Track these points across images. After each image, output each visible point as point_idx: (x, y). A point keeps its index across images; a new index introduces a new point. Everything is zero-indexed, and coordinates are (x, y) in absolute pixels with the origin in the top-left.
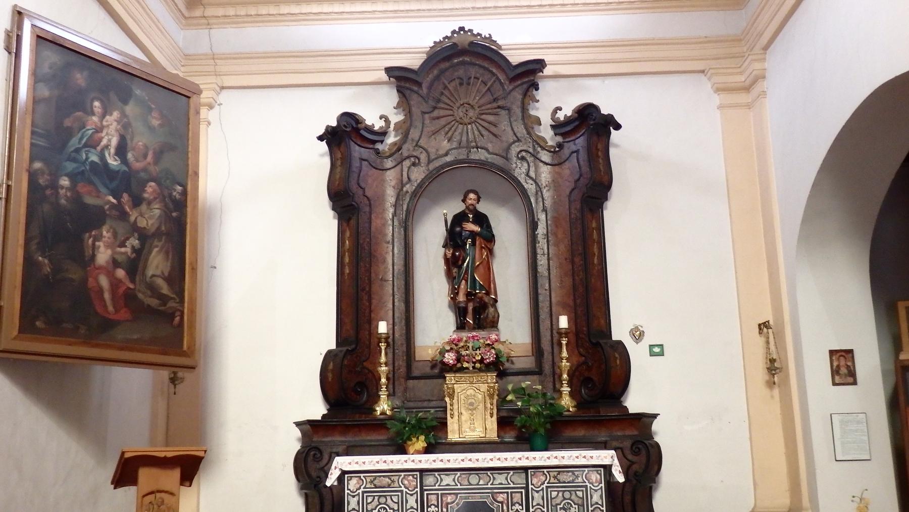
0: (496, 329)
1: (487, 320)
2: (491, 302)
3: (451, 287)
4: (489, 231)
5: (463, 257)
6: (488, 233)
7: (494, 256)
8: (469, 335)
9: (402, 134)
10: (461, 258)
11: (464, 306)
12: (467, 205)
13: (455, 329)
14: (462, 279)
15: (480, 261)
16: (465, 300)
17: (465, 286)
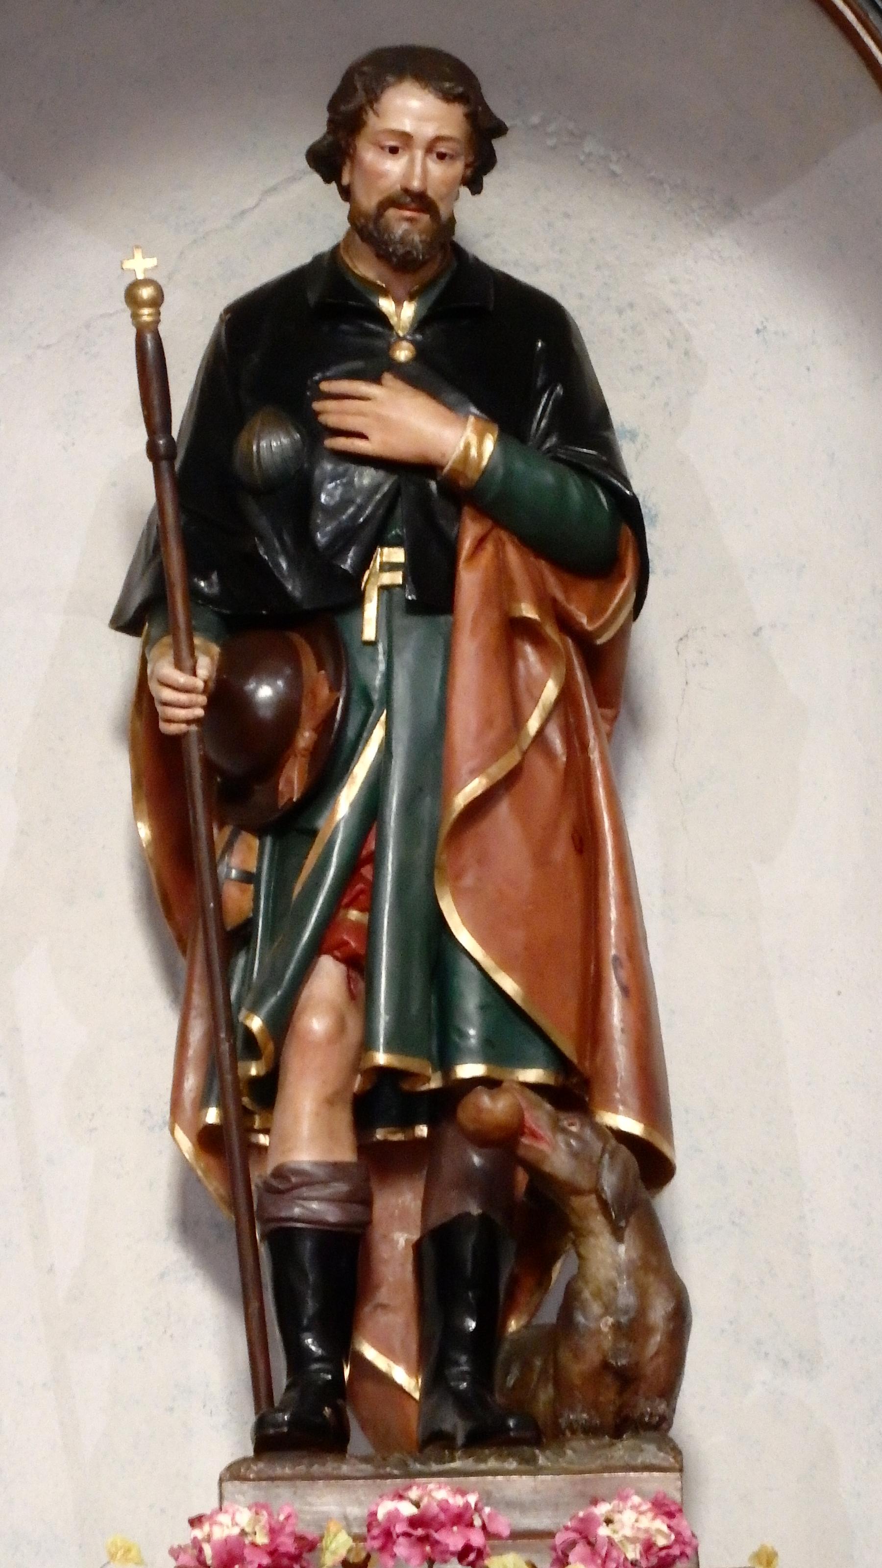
0: (651, 1453)
1: (565, 1355)
2: (609, 1182)
3: (197, 1032)
4: (579, 468)
5: (325, 725)
6: (575, 489)
7: (636, 721)
8: (384, 1508)
9: (351, 1219)
10: (305, 737)
11: (331, 1214)
12: (369, 202)
13: (249, 1451)
14: (317, 948)
15: (499, 770)
16: (346, 1154)
17: (341, 1026)
